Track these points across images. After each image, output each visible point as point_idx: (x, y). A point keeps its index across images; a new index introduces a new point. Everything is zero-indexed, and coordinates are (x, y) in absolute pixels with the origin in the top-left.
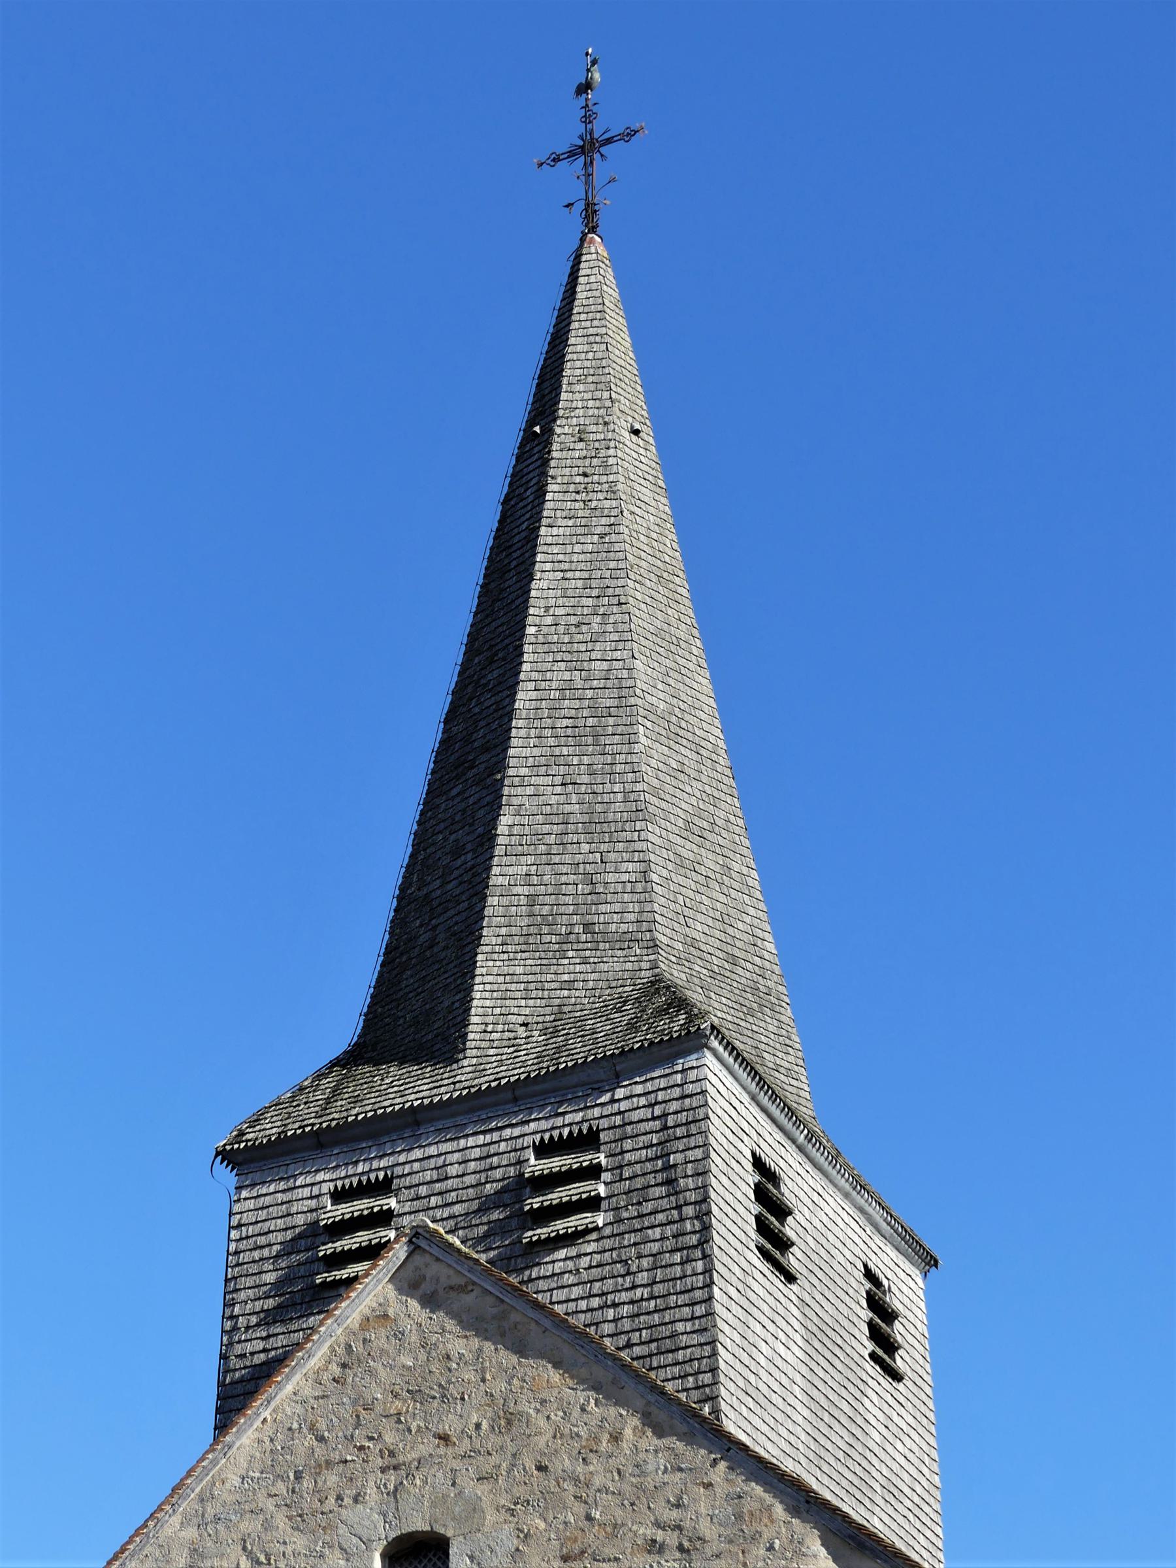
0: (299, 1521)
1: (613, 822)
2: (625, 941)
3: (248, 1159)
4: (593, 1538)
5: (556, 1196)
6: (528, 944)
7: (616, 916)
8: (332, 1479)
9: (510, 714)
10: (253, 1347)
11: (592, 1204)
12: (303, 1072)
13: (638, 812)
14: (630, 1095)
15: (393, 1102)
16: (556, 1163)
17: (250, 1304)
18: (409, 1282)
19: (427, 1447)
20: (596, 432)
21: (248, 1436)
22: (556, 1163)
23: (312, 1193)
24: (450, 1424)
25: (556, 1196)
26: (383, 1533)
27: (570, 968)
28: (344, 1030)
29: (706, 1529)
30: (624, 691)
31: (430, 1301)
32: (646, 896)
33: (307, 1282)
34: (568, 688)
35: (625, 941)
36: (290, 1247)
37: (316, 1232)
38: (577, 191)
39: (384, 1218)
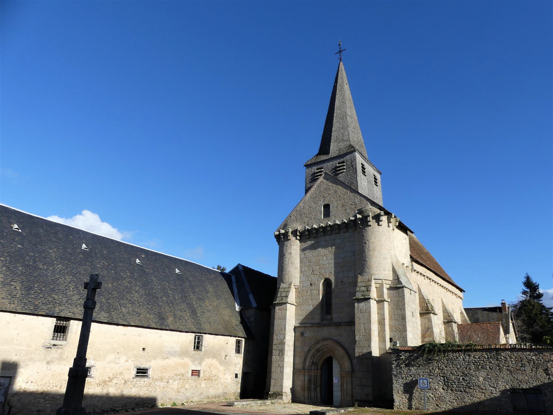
0: (314, 203)
1: (345, 128)
2: (347, 141)
3: (307, 166)
4: (345, 204)
5: (340, 168)
6: (336, 141)
7: (346, 138)
8: (317, 199)
9: (333, 116)
10: (309, 185)
11: (344, 169)
12: (312, 157)
13: (348, 126)
14: (348, 157)
15: (322, 159)
16: (340, 165)
17: (308, 181)
18: (325, 178)
19: (327, 195)
20: (342, 84)
21: (308, 195)
22: (340, 165)
23: (314, 169)
24: (330, 193)
25: (340, 168)
26: (323, 204)
27: (341, 144)
28: (317, 152)
29: (357, 202)
30: (346, 113)
31: (327, 180)
32: (349, 135)
33: (314, 178)
34: (340, 113)
35: (347, 141)
36: (312, 175)
37: (315, 173)
38: (339, 57)
39: (344, 169)
